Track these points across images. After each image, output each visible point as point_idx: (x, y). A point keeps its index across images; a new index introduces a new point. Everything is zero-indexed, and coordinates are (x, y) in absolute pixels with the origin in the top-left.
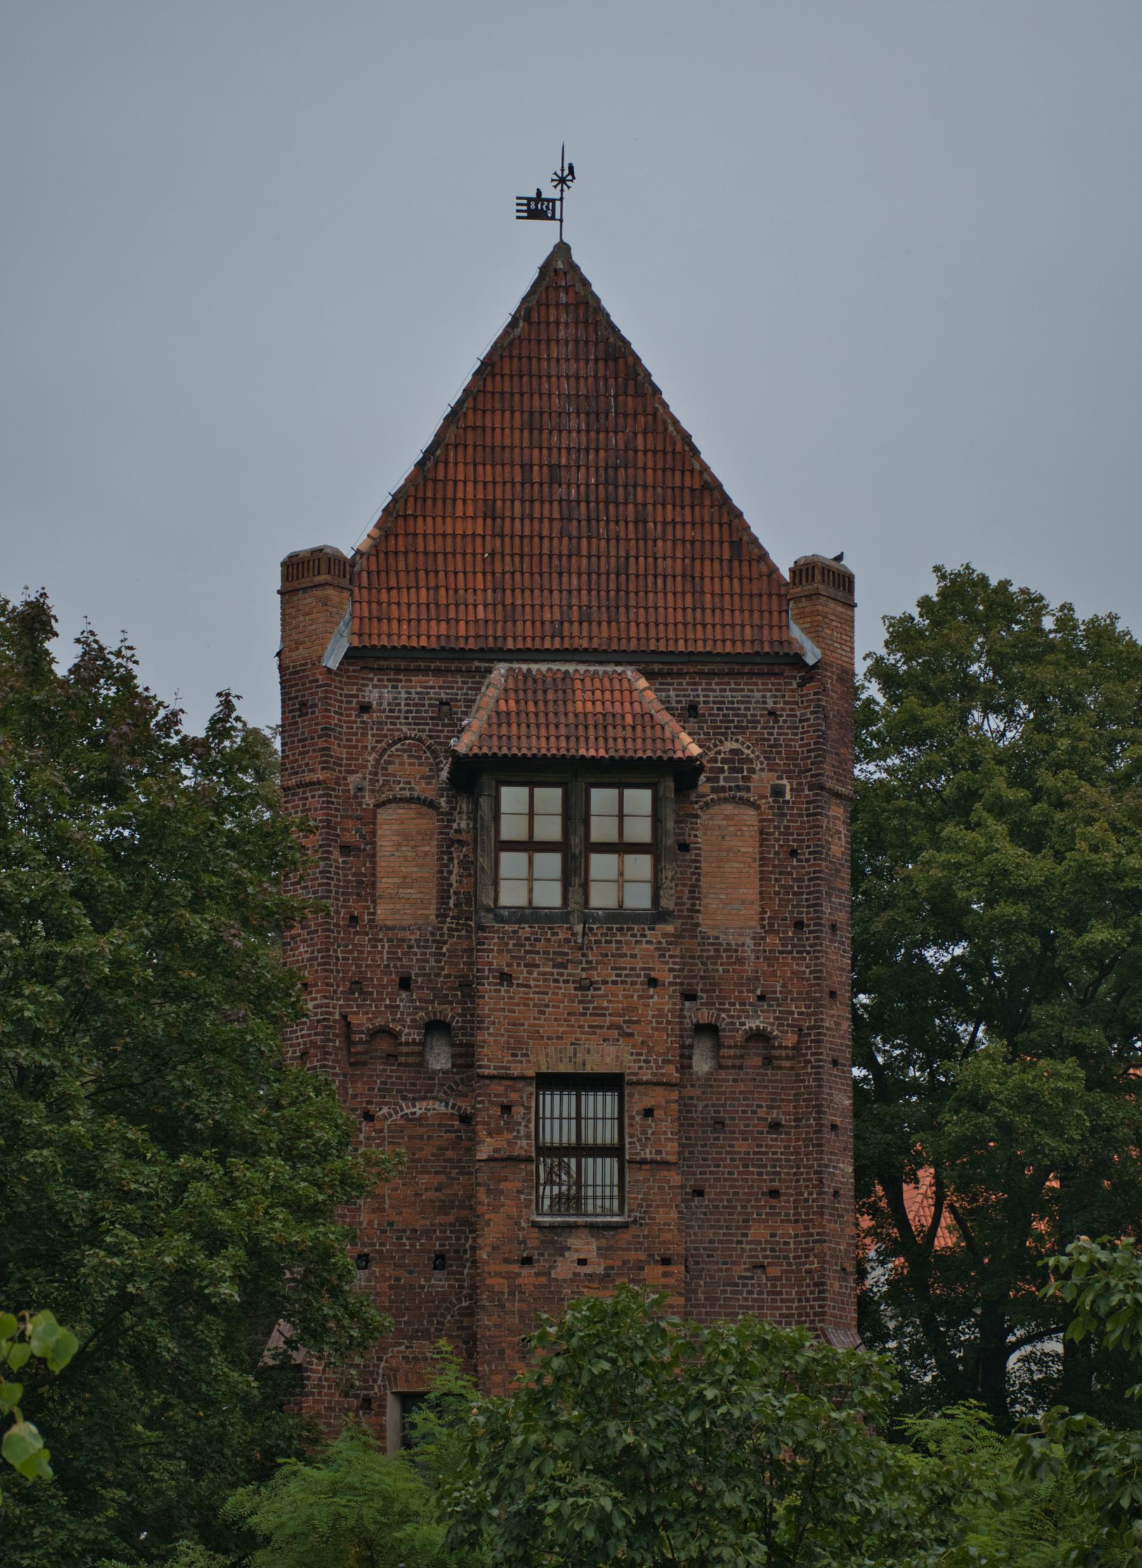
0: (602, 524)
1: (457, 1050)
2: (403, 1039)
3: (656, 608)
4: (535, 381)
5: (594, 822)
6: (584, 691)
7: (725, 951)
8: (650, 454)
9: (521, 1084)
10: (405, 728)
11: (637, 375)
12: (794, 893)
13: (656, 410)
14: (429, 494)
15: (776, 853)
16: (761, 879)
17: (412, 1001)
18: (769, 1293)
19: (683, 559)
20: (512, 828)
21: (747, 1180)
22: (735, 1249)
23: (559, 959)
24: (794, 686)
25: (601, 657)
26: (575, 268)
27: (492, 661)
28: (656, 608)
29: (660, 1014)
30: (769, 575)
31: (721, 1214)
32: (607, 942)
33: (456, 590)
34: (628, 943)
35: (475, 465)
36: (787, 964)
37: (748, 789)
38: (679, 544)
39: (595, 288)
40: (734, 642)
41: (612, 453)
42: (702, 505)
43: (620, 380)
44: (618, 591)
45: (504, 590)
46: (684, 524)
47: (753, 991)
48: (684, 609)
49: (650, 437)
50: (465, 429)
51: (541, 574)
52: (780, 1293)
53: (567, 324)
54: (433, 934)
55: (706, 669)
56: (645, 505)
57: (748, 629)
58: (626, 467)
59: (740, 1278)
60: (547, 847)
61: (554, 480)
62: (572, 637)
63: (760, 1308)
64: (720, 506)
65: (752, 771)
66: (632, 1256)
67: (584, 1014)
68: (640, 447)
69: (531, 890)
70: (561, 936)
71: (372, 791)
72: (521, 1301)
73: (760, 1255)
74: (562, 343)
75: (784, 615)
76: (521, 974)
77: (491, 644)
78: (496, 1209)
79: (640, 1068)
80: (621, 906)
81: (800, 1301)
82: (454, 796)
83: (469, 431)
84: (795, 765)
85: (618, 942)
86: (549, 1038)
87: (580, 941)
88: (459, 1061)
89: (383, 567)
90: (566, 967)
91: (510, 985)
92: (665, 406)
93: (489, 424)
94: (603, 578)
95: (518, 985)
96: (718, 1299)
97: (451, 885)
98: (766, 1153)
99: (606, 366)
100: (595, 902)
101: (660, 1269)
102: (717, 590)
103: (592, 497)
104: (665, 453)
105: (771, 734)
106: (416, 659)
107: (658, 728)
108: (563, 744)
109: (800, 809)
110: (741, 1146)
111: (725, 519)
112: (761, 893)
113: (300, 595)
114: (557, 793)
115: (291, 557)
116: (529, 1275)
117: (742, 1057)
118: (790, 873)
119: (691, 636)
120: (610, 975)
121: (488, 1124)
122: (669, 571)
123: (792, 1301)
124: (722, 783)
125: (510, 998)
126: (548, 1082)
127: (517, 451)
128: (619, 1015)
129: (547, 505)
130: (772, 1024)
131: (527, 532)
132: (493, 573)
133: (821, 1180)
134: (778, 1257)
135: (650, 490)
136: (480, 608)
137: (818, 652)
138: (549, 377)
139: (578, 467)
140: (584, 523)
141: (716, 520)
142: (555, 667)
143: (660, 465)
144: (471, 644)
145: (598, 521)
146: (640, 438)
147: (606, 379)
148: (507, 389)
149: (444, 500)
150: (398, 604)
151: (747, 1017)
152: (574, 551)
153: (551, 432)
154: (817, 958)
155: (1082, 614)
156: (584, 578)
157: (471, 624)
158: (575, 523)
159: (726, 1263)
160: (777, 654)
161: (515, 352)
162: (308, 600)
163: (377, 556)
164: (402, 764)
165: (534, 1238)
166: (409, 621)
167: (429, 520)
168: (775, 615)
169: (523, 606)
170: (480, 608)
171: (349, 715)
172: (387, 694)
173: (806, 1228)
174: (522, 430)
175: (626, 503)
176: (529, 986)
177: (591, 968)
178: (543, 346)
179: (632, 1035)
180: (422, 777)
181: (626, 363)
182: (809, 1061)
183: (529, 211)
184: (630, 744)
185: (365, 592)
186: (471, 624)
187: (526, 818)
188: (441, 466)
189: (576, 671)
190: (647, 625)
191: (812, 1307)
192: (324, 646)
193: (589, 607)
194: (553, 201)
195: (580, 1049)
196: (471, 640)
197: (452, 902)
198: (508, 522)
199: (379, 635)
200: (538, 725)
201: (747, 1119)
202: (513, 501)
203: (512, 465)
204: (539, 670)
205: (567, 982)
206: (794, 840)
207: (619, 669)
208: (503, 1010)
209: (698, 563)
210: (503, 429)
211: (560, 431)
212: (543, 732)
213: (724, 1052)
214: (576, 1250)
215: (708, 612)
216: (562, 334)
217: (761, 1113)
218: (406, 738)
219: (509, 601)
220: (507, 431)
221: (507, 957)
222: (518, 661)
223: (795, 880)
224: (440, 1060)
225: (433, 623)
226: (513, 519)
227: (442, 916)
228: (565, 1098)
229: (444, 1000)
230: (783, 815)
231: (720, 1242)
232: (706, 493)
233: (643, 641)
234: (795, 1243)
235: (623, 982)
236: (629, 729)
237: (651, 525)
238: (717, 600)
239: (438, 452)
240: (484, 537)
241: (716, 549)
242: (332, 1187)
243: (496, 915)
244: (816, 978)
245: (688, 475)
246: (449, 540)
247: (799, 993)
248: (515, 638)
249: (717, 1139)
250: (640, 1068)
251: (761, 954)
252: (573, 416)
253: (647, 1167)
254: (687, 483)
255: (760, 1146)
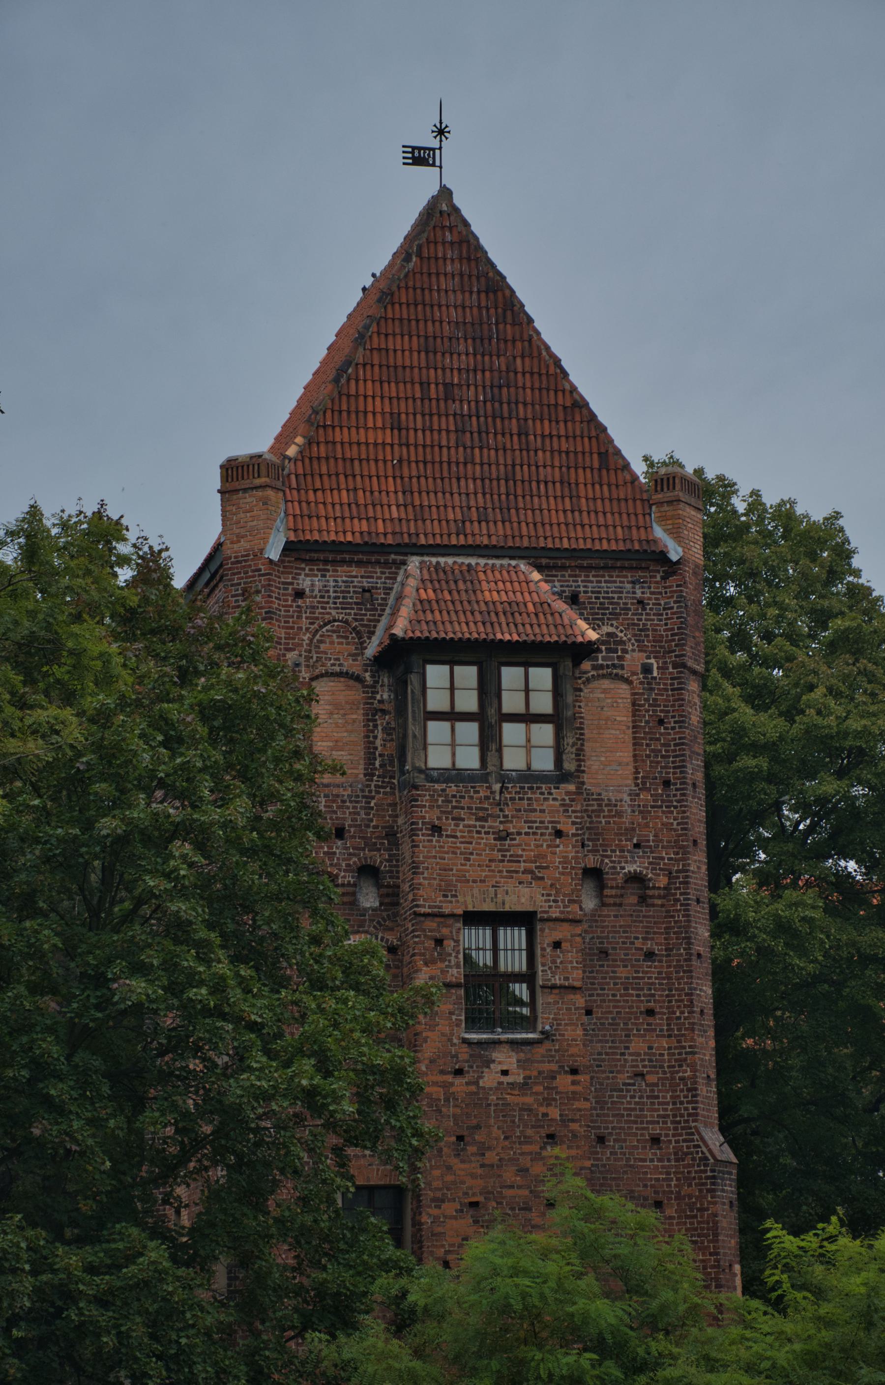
0: (491, 436)
1: (384, 891)
2: (340, 881)
3: (541, 510)
4: (428, 309)
5: (505, 695)
6: (488, 582)
7: (606, 805)
8: (528, 376)
9: (450, 921)
10: (333, 612)
11: (513, 306)
12: (662, 757)
13: (531, 337)
14: (344, 407)
15: (647, 722)
16: (634, 744)
17: (347, 848)
18: (648, 1097)
19: (561, 468)
20: (436, 701)
21: (627, 1001)
22: (620, 1060)
23: (481, 814)
24: (658, 579)
25: (499, 553)
26: (457, 210)
27: (406, 554)
28: (541, 510)
29: (565, 861)
30: (632, 483)
31: (608, 1030)
32: (520, 799)
33: (372, 492)
34: (537, 800)
35: (381, 382)
36: (657, 817)
37: (622, 667)
38: (556, 454)
39: (473, 228)
40: (609, 541)
41: (496, 374)
42: (573, 421)
43: (500, 310)
44: (508, 495)
45: (412, 493)
46: (559, 437)
47: (631, 840)
48: (565, 511)
49: (527, 360)
50: (371, 350)
51: (442, 479)
52: (657, 1097)
53: (452, 260)
54: (363, 791)
55: (585, 563)
56: (526, 420)
57: (619, 529)
58: (508, 387)
59: (625, 1084)
60: (466, 717)
61: (449, 397)
62: (473, 535)
63: (641, 1110)
64: (589, 422)
65: (625, 651)
66: (547, 1067)
67: (503, 861)
68: (520, 369)
69: (454, 754)
70: (482, 794)
71: (307, 666)
72: (455, 1106)
73: (640, 1064)
74: (449, 276)
75: (647, 517)
76: (450, 826)
77: (407, 540)
78: (432, 1027)
79: (550, 907)
80: (529, 768)
81: (674, 1103)
82: (377, 671)
83: (375, 352)
84: (660, 647)
85: (529, 799)
86: (474, 881)
87: (497, 798)
88: (387, 900)
89: (308, 471)
90: (486, 821)
91: (440, 836)
92: (538, 333)
93: (391, 347)
94: (495, 483)
95: (447, 836)
96: (607, 1103)
97: (376, 748)
98: (643, 978)
99: (487, 296)
100: (507, 765)
101: (570, 1078)
102: (591, 495)
103: (482, 413)
104: (540, 375)
105: (640, 620)
106: (342, 552)
107: (557, 615)
108: (482, 629)
109: (665, 684)
110: (622, 972)
111: (593, 434)
112: (635, 756)
113: (241, 494)
114: (473, 670)
115: (229, 461)
116: (461, 1085)
117: (622, 896)
118: (658, 739)
119: (572, 535)
120: (523, 828)
121: (423, 955)
122: (550, 478)
123: (668, 1103)
124: (600, 662)
125: (440, 847)
126: (473, 919)
127: (416, 370)
128: (531, 862)
129: (443, 419)
130: (647, 868)
131: (428, 442)
132: (402, 478)
133: (691, 1001)
134: (655, 1067)
135: (530, 407)
136: (394, 508)
137: (680, 550)
138: (440, 306)
139: (468, 386)
140: (476, 435)
141: (586, 433)
142: (460, 560)
143: (537, 385)
144: (390, 540)
145: (487, 433)
146: (519, 361)
147: (488, 309)
148: (405, 316)
149: (357, 412)
150: (324, 503)
151: (626, 862)
152: (469, 460)
153: (443, 354)
154: (684, 812)
155: (770, 499)
156: (479, 482)
157: (388, 522)
158: (468, 435)
159: (612, 1072)
160: (646, 551)
161: (411, 284)
162: (249, 499)
163: (303, 461)
164: (332, 643)
165: (464, 1053)
166: (335, 519)
167: (345, 430)
168: (640, 517)
169: (430, 507)
170: (394, 508)
171: (287, 600)
172: (318, 583)
173: (679, 1041)
174: (419, 352)
175: (510, 418)
176: (456, 837)
177: (507, 822)
178: (434, 279)
179: (542, 878)
180: (349, 655)
181: (504, 295)
182: (679, 900)
183: (413, 158)
184: (537, 630)
185: (295, 492)
186: (388, 522)
187: (448, 692)
188: (353, 383)
189: (477, 564)
190: (535, 524)
191: (686, 1109)
192: (265, 540)
193: (485, 509)
194: (434, 150)
195: (499, 890)
196: (389, 536)
197: (377, 764)
198: (412, 432)
199: (311, 531)
200: (456, 612)
201: (627, 949)
202: (415, 414)
203: (413, 383)
204: (446, 563)
205: (487, 833)
206: (661, 711)
207: (513, 563)
208: (435, 857)
209: (572, 471)
210: (403, 351)
211: (451, 354)
212: (463, 619)
213: (607, 892)
214: (500, 1063)
215: (585, 514)
216: (449, 268)
217: (638, 944)
218: (335, 621)
219: (417, 503)
220: (407, 353)
221: (437, 812)
222: (428, 555)
223: (663, 745)
224: (369, 899)
225: (356, 521)
226: (416, 430)
227: (369, 775)
228: (516, 932)
229: (373, 847)
230: (652, 689)
231: (607, 1054)
232: (577, 410)
233: (533, 539)
234: (669, 1054)
235: (534, 834)
236: (533, 616)
237: (532, 437)
238: (591, 504)
239: (350, 371)
240: (392, 445)
241: (588, 459)
242: (393, 1015)
243: (427, 775)
244: (682, 829)
245: (560, 394)
246: (363, 447)
247: (668, 842)
248: (426, 535)
249: (602, 966)
250: (550, 907)
251: (636, 808)
252: (462, 341)
253: (557, 991)
254: (560, 402)
255: (637, 972)
